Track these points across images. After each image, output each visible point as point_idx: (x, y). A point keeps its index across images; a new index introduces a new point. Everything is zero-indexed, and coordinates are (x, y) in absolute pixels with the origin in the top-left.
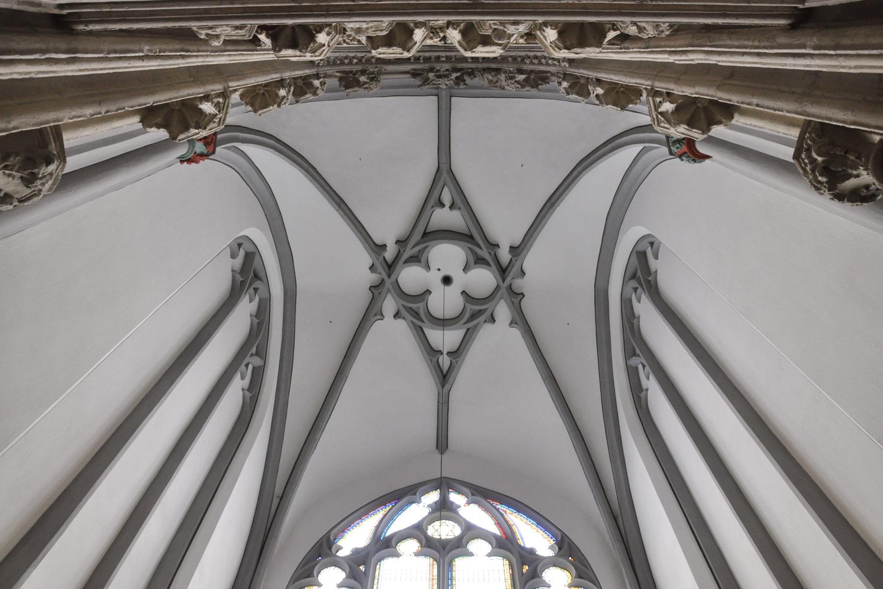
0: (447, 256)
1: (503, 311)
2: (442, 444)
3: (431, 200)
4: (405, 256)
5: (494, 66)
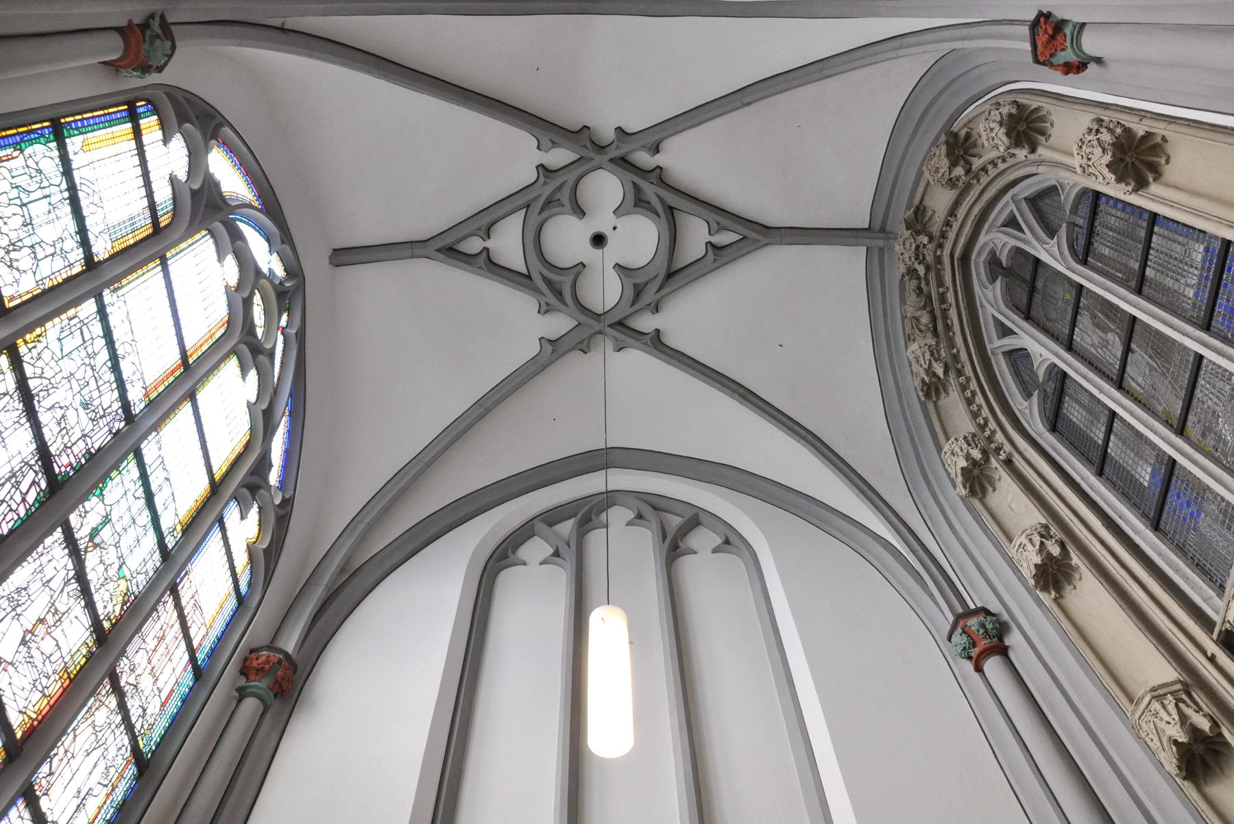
0: (639, 240)
1: (560, 324)
2: (343, 256)
3: (719, 214)
4: (643, 184)
5: (940, 326)
